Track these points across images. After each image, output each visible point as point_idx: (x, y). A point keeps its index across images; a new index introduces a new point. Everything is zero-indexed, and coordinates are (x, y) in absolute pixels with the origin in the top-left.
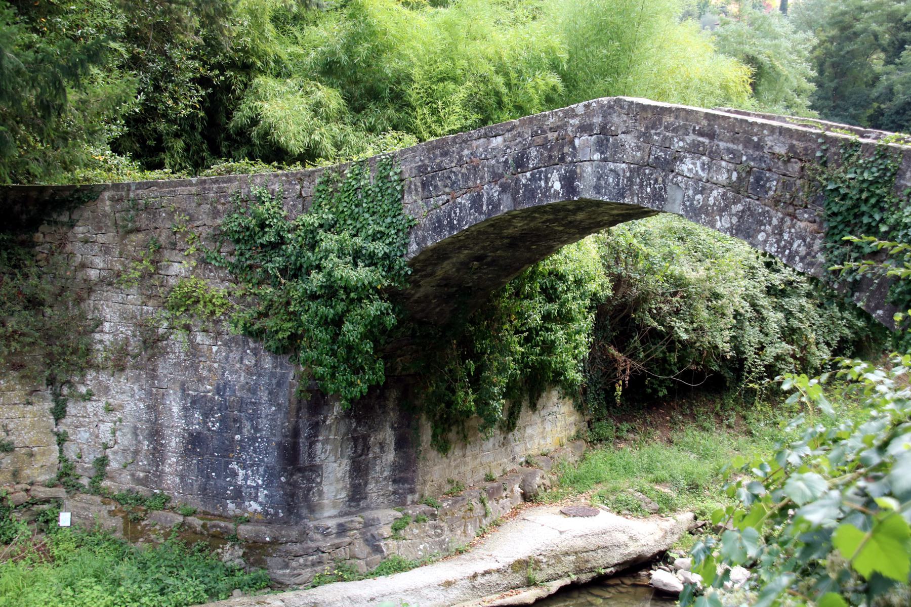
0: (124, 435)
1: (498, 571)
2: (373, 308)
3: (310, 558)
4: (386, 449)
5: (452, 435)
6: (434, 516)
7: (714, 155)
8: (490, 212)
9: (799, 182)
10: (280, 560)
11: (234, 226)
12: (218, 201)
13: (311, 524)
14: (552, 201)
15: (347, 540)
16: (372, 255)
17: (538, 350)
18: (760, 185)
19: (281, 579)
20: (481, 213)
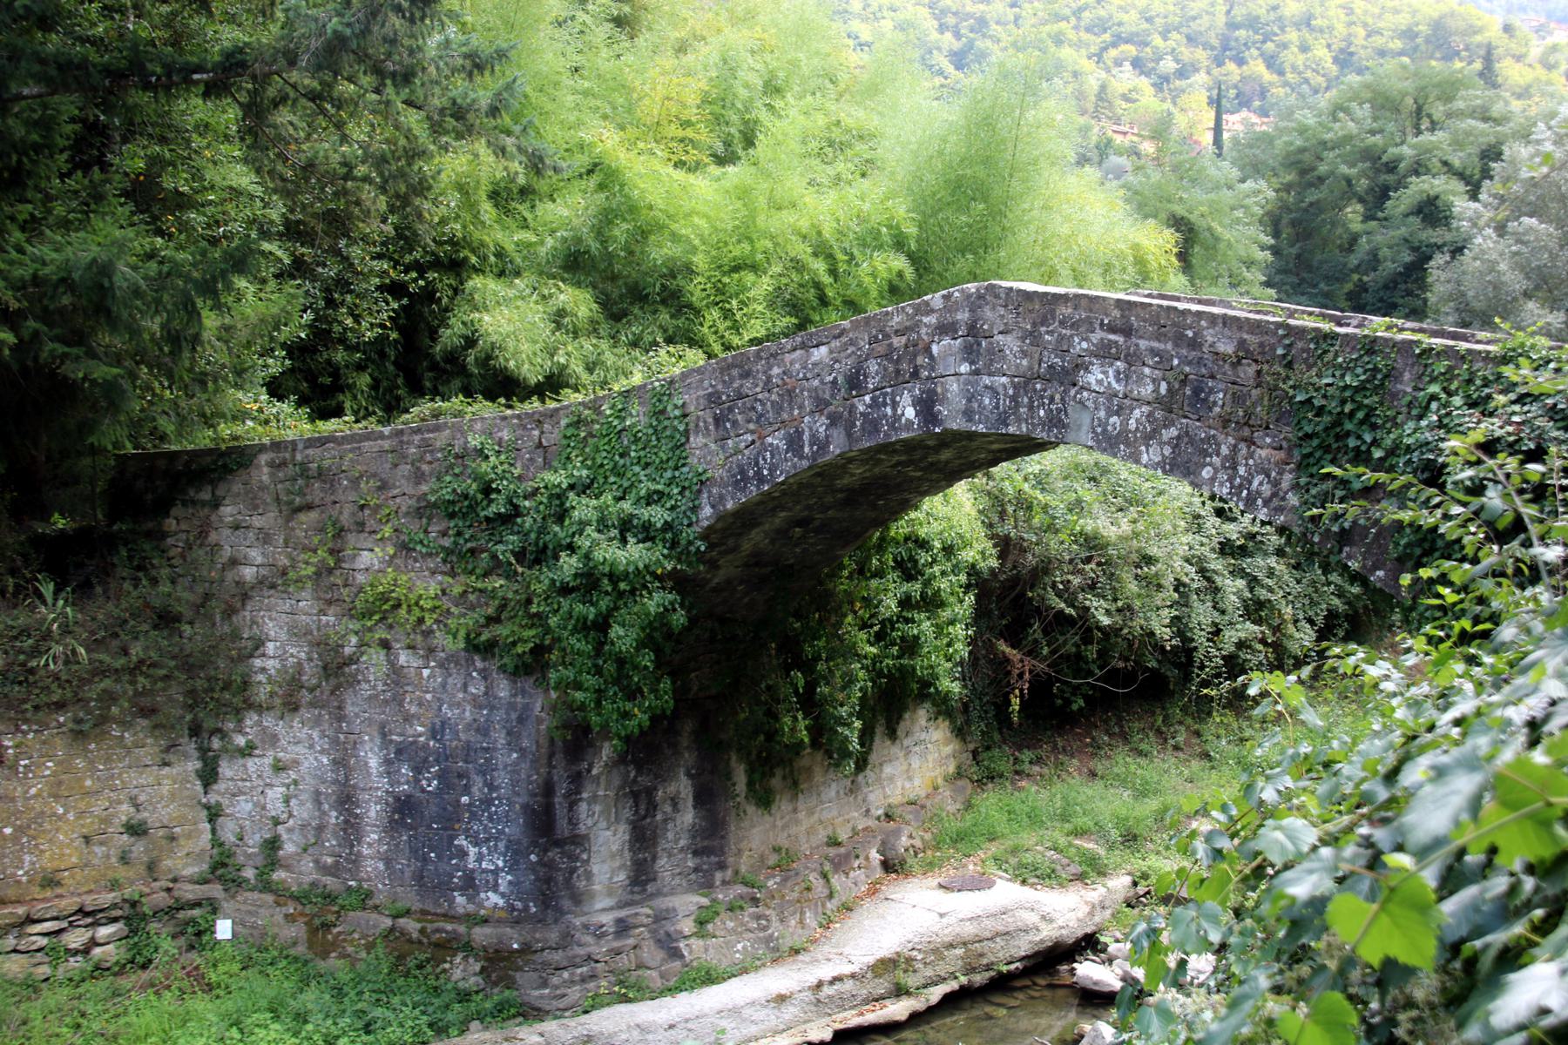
0: (302, 804)
1: (853, 976)
2: (654, 602)
3: (579, 971)
4: (681, 806)
5: (776, 782)
6: (755, 901)
7: (1133, 359)
8: (814, 456)
10: (534, 975)
13: (577, 922)
14: (904, 435)
15: (631, 941)
18: (1200, 399)
19: (537, 1004)
20: (801, 457)
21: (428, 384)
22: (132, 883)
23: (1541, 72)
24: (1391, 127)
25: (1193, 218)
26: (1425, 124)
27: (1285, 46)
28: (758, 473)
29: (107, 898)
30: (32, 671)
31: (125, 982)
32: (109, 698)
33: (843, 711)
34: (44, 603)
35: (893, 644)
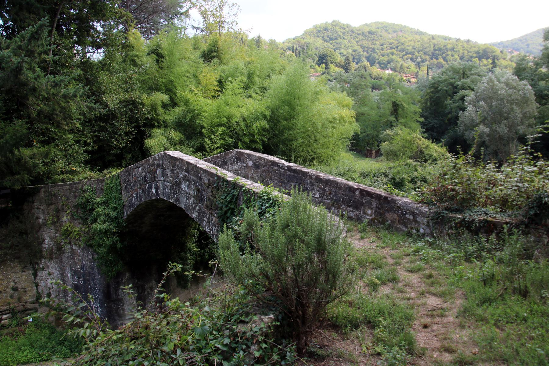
12: (75, 192)
14: (154, 198)
22: (14, 303)
23: (509, 62)
25: (397, 102)
26: (466, 76)
27: (448, 55)
29: (5, 308)
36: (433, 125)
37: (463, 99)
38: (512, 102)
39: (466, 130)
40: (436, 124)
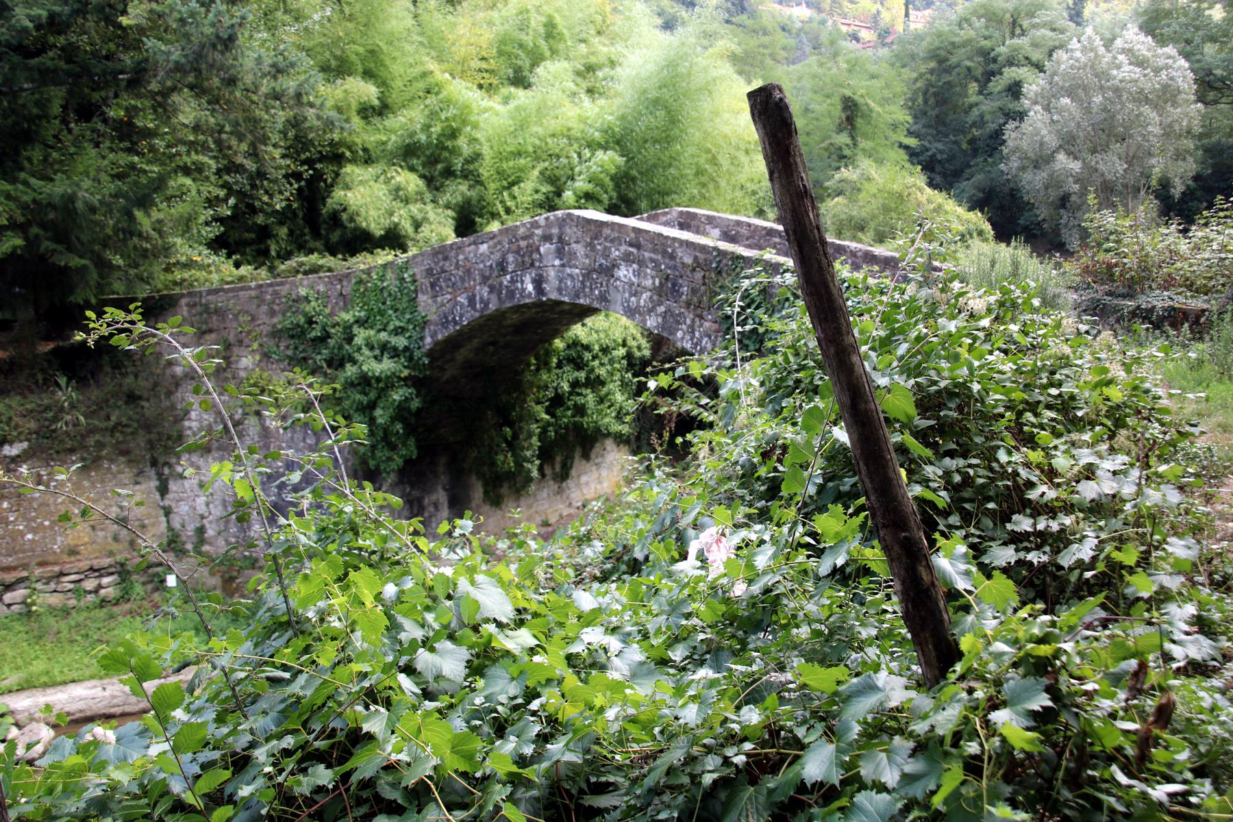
0: (216, 507)
2: (397, 396)
5: (504, 490)
7: (641, 263)
8: (482, 310)
9: (703, 288)
11: (287, 324)
12: (273, 302)
14: (527, 301)
16: (395, 349)
17: (569, 413)
18: (675, 291)
20: (476, 310)
21: (323, 232)
22: (121, 552)
24: (997, 34)
25: (856, 98)
26: (1018, 31)
28: (454, 318)
29: (106, 562)
30: (54, 431)
31: (116, 610)
32: (100, 445)
33: (528, 453)
34: (61, 389)
35: (568, 409)
36: (934, 155)
37: (1015, 90)
38: (1142, 98)
39: (1023, 168)
40: (941, 152)
